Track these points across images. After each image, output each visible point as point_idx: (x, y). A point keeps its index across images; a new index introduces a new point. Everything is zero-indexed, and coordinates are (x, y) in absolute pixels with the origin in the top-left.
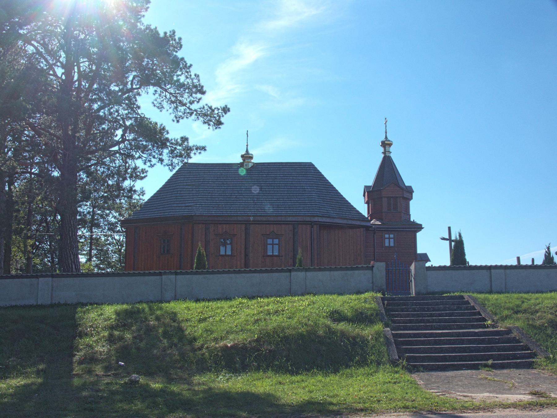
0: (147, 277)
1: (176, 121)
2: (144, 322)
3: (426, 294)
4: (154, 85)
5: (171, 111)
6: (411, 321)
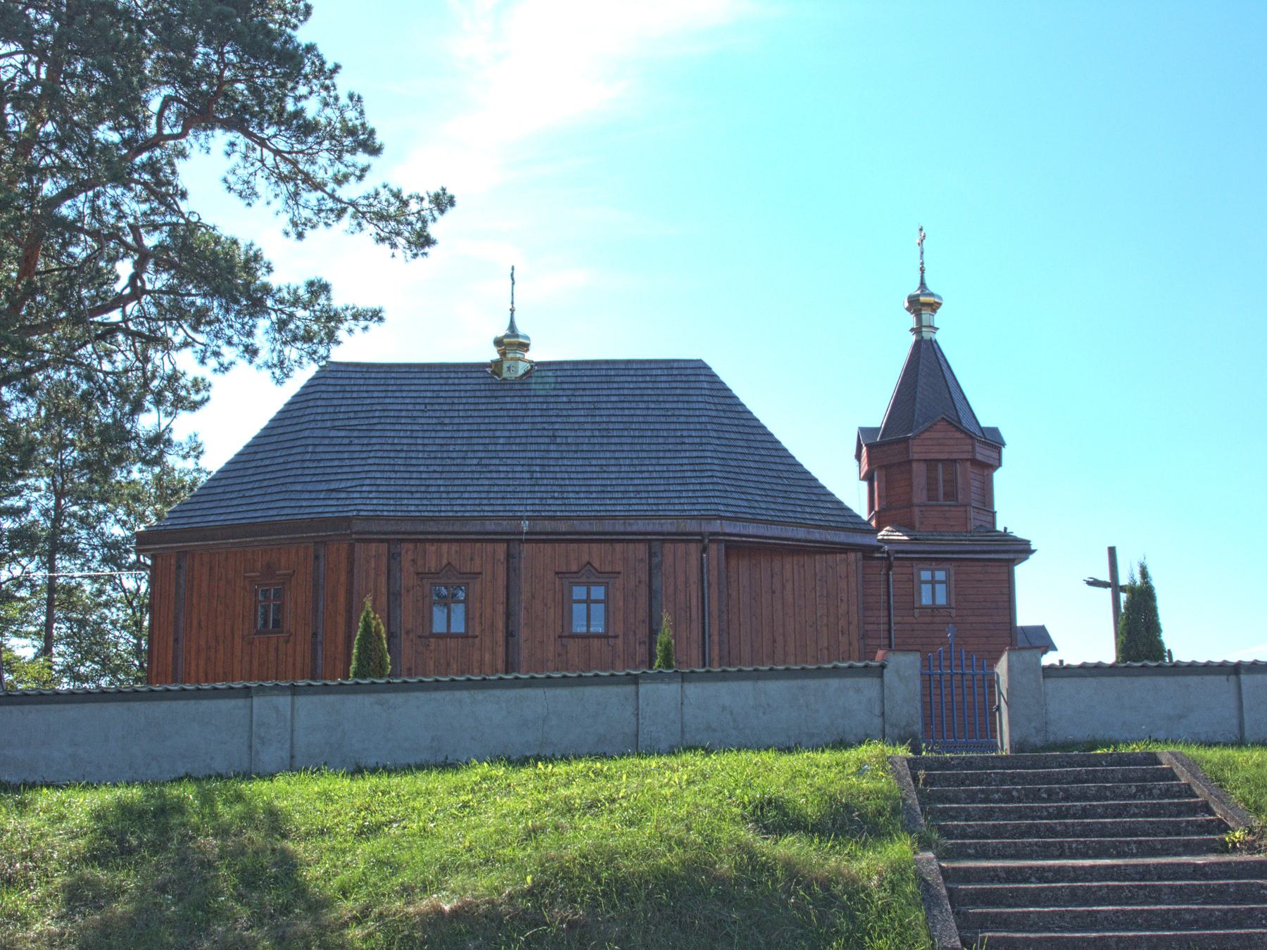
0: (205, 703)
1: (293, 236)
2: (191, 838)
3: (1044, 749)
4: (228, 126)
5: (279, 204)
6: (998, 832)
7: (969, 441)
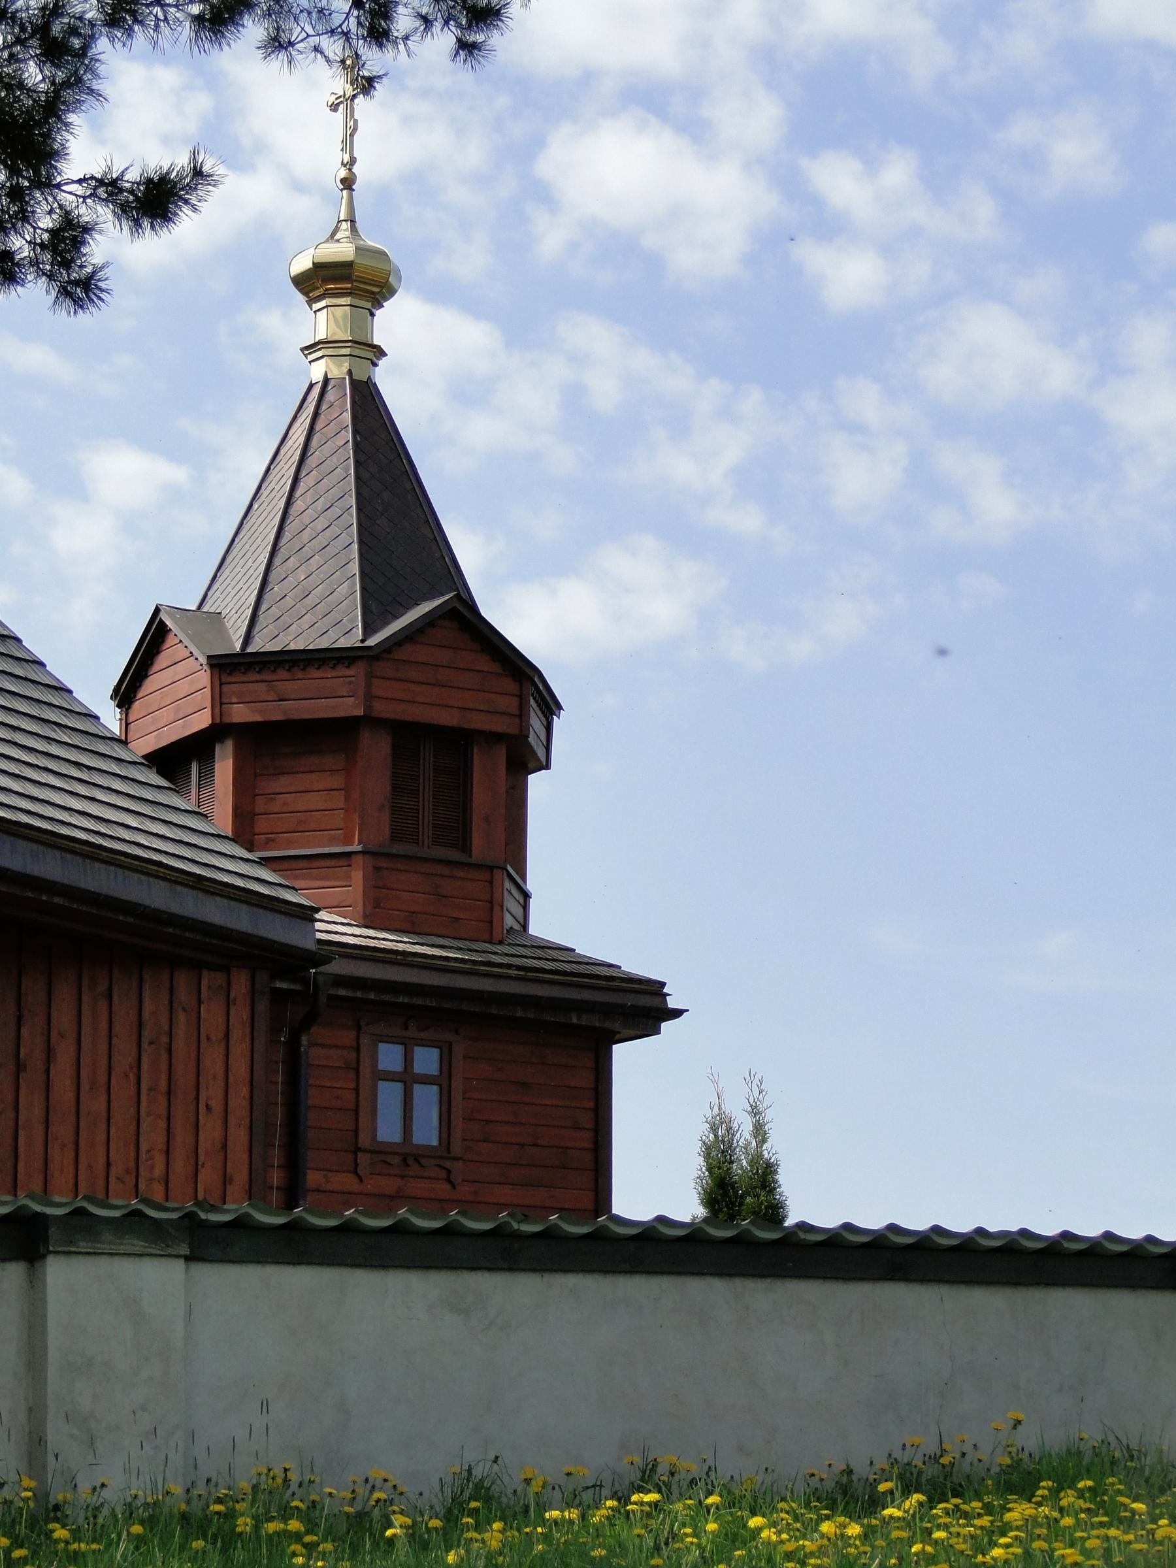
7: (509, 685)
